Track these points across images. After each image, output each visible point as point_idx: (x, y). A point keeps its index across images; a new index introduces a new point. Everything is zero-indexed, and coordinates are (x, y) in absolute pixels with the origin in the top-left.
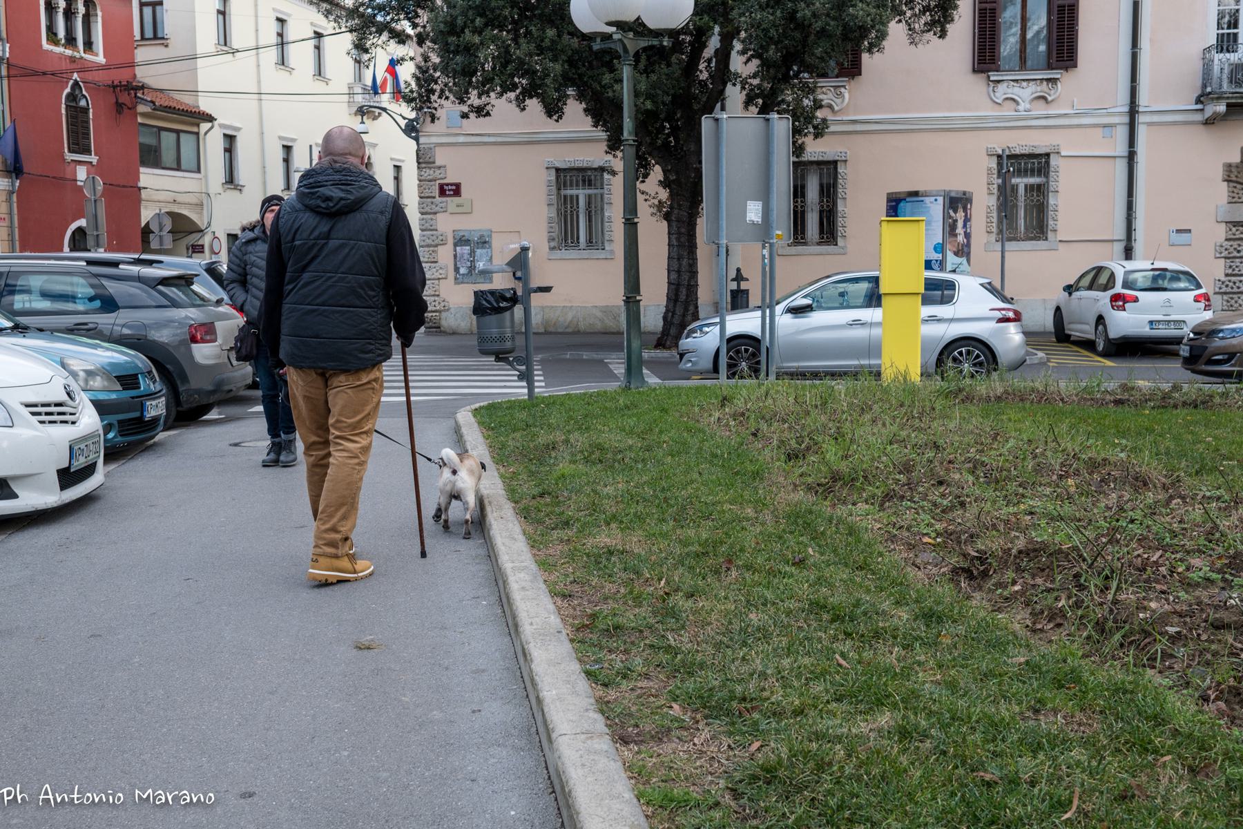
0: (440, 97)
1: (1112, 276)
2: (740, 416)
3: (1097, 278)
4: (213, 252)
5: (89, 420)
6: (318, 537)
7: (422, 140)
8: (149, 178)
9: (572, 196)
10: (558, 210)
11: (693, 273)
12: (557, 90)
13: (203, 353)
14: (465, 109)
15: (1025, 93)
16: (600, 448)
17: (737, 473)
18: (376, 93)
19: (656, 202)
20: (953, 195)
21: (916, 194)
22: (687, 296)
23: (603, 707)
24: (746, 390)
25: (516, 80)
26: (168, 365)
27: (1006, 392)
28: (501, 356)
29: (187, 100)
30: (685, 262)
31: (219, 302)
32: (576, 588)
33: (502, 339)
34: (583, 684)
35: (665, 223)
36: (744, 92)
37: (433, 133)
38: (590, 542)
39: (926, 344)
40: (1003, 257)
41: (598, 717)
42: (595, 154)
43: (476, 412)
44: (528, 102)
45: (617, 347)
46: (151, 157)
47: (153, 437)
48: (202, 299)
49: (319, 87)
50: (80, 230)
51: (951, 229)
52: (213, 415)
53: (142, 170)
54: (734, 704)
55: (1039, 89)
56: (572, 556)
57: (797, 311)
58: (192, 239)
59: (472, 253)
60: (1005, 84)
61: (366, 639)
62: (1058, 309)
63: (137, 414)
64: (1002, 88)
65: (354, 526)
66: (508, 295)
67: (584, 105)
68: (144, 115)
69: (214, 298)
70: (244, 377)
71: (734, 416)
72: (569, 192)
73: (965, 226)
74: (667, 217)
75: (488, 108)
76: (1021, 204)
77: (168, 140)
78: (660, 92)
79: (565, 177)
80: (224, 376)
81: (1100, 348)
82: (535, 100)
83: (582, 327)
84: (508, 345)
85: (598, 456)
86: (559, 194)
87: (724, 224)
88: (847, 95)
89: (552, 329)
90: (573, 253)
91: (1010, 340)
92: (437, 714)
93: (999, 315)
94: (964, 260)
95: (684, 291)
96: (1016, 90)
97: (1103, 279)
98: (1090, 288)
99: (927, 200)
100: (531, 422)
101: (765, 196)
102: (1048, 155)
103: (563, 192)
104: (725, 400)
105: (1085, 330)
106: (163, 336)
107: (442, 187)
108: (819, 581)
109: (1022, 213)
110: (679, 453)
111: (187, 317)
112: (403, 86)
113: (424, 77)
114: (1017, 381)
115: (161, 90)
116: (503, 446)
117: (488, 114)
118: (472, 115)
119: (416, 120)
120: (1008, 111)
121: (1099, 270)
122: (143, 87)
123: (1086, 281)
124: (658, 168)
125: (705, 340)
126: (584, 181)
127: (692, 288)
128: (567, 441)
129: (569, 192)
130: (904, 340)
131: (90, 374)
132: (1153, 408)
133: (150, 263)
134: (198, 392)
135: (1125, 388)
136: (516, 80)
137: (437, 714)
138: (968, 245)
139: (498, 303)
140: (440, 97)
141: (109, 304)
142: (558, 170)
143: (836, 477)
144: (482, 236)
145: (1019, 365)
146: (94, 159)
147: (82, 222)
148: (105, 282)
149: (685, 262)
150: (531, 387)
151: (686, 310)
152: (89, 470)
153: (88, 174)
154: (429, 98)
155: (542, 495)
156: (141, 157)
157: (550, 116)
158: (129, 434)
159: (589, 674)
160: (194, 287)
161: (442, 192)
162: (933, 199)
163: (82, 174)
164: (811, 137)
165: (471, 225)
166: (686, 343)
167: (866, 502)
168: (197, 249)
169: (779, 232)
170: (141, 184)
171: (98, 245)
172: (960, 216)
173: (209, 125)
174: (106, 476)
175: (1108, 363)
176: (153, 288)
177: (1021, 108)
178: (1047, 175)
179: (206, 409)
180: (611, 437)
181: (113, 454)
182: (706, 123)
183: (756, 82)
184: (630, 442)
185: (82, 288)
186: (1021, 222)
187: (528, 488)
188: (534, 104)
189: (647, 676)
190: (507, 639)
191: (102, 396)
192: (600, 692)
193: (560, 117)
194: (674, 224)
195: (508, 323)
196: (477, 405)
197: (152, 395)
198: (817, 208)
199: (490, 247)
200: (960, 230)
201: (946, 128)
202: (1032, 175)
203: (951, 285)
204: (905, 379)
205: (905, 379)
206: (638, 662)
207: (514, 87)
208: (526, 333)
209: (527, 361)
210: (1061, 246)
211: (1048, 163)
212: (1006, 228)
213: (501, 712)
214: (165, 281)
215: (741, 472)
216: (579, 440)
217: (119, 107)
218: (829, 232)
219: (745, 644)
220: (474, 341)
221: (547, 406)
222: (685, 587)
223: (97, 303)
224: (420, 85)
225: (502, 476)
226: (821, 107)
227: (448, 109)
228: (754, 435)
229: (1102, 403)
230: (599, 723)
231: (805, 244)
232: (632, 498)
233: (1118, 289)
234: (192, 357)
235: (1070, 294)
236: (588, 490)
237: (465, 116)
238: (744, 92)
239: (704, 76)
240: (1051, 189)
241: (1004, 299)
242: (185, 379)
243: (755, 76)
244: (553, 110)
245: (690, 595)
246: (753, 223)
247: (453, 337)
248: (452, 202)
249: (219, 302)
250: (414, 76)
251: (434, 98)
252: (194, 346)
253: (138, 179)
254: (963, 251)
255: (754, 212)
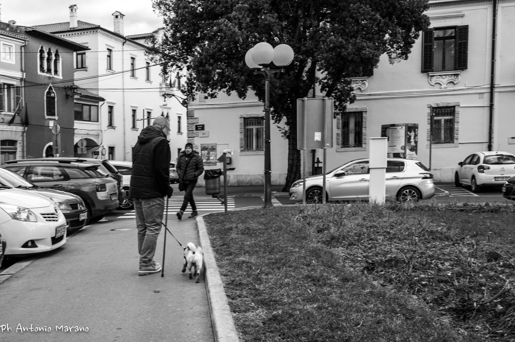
0: (196, 90)
1: (479, 158)
2: (305, 218)
3: (473, 159)
4: (103, 155)
5: (62, 220)
6: (141, 260)
7: (189, 107)
8: (78, 125)
9: (250, 129)
10: (245, 135)
11: (299, 160)
12: (243, 88)
13: (101, 196)
14: (206, 95)
15: (444, 81)
16: (248, 229)
17: (297, 237)
18: (171, 87)
19: (284, 131)
20: (409, 125)
21: (394, 125)
22: (296, 170)
23: (230, 304)
24: (309, 208)
25: (226, 83)
26: (88, 199)
27: (416, 207)
28: (214, 195)
29: (94, 93)
30: (295, 156)
31: (107, 176)
32: (230, 273)
33: (215, 189)
34: (225, 298)
35: (287, 140)
36: (321, 86)
37: (193, 105)
38: (237, 260)
39: (388, 190)
40: (430, 151)
41: (228, 306)
42: (259, 112)
43: (204, 217)
44: (231, 92)
45: (261, 192)
46: (79, 116)
47: (82, 227)
48: (101, 174)
49: (148, 85)
50: (50, 147)
51: (408, 140)
52: (103, 220)
53: (75, 121)
54: (271, 303)
55: (450, 78)
56: (230, 264)
57: (338, 176)
58: (94, 149)
59: (208, 153)
60: (436, 77)
61: (158, 290)
62: (457, 173)
63: (76, 219)
64: (434, 79)
65: (153, 255)
66: (218, 172)
67: (255, 92)
68: (77, 99)
69: (106, 174)
70: (116, 205)
71: (303, 217)
72: (249, 127)
73: (415, 138)
74: (288, 137)
75: (216, 94)
76: (443, 128)
77: (86, 108)
78: (285, 86)
79: (247, 121)
80: (108, 204)
81: (473, 189)
82: (234, 91)
83: (253, 183)
84: (217, 191)
85: (248, 232)
86: (245, 129)
87: (305, 141)
88: (367, 84)
89: (241, 184)
90: (250, 153)
91: (428, 186)
92: (179, 309)
93: (423, 176)
94: (414, 153)
95: (295, 168)
96: (441, 79)
97: (475, 160)
98: (470, 163)
99: (399, 128)
100: (224, 220)
101: (322, 130)
102: (454, 107)
103: (247, 127)
104: (301, 211)
105: (467, 181)
106: (86, 189)
107: (196, 126)
108: (312, 270)
109: (443, 132)
110: (278, 230)
111: (95, 182)
112: (181, 86)
113: (190, 83)
114: (429, 203)
115: (84, 89)
116: (213, 229)
117: (216, 97)
118: (209, 97)
119: (187, 99)
120: (437, 88)
121: (474, 156)
122: (77, 88)
123: (468, 161)
124: (285, 117)
125: (299, 189)
126: (258, 122)
127: (298, 166)
128: (236, 227)
129: (249, 127)
130: (379, 187)
131: (61, 204)
132: (475, 213)
133: (81, 161)
134: (99, 210)
135: (465, 205)
136: (226, 83)
137: (179, 309)
138: (416, 146)
139: (214, 174)
140: (196, 90)
141: (67, 177)
142: (245, 118)
143: (333, 238)
144: (213, 146)
145: (430, 197)
146: (56, 118)
147: (51, 144)
148: (66, 169)
149: (295, 156)
150: (226, 208)
151: (296, 175)
152: (61, 238)
153: (54, 124)
154: (192, 91)
155: (223, 245)
156: (75, 116)
157: (240, 97)
158: (74, 226)
159: (228, 296)
160: (99, 170)
161: (197, 128)
162: (400, 127)
163: (51, 124)
164: (349, 102)
165: (206, 142)
166: (293, 189)
167: (342, 247)
168: (97, 153)
169: (328, 144)
170: (75, 127)
171: (57, 153)
172: (412, 134)
173: (103, 102)
174: (67, 240)
175: (476, 195)
176: (83, 171)
177: (442, 87)
178: (454, 115)
179: (101, 218)
180: (253, 225)
181: (70, 233)
182: (299, 102)
183: (326, 81)
184: (260, 227)
185: (56, 171)
186: (443, 136)
187: (219, 243)
188: (234, 93)
189: (247, 297)
190: (204, 289)
191: (65, 212)
192: (231, 300)
193: (245, 98)
194: (291, 140)
195: (217, 182)
196: (205, 215)
197: (82, 212)
198: (354, 132)
199: (216, 151)
200: (412, 140)
201: (409, 96)
202: (447, 115)
203: (403, 164)
204: (375, 203)
205: (375, 203)
206: (245, 293)
207: (225, 87)
208: (224, 186)
209: (224, 197)
210: (460, 145)
211: (454, 110)
212: (435, 137)
213: (199, 308)
214: (88, 168)
215: (299, 236)
216: (241, 226)
217: (67, 96)
218: (359, 142)
219: (280, 287)
220: (204, 190)
221: (232, 214)
222: (266, 272)
223: (62, 177)
224: (188, 86)
225: (210, 239)
226: (353, 90)
227: (199, 95)
228: (308, 224)
229: (455, 211)
230: (228, 307)
231: (349, 147)
232: (255, 245)
233: (481, 163)
234: (96, 197)
235: (462, 166)
236: (240, 243)
237: (206, 98)
238: (321, 86)
239: (305, 78)
240: (456, 121)
241: (425, 169)
242: (94, 205)
243: (325, 79)
244: (242, 95)
245: (267, 274)
246: (317, 141)
247: (200, 188)
248: (200, 132)
249: (107, 176)
250: (186, 82)
251: (194, 91)
252: (98, 193)
253: (73, 126)
254: (414, 149)
255: (318, 136)
